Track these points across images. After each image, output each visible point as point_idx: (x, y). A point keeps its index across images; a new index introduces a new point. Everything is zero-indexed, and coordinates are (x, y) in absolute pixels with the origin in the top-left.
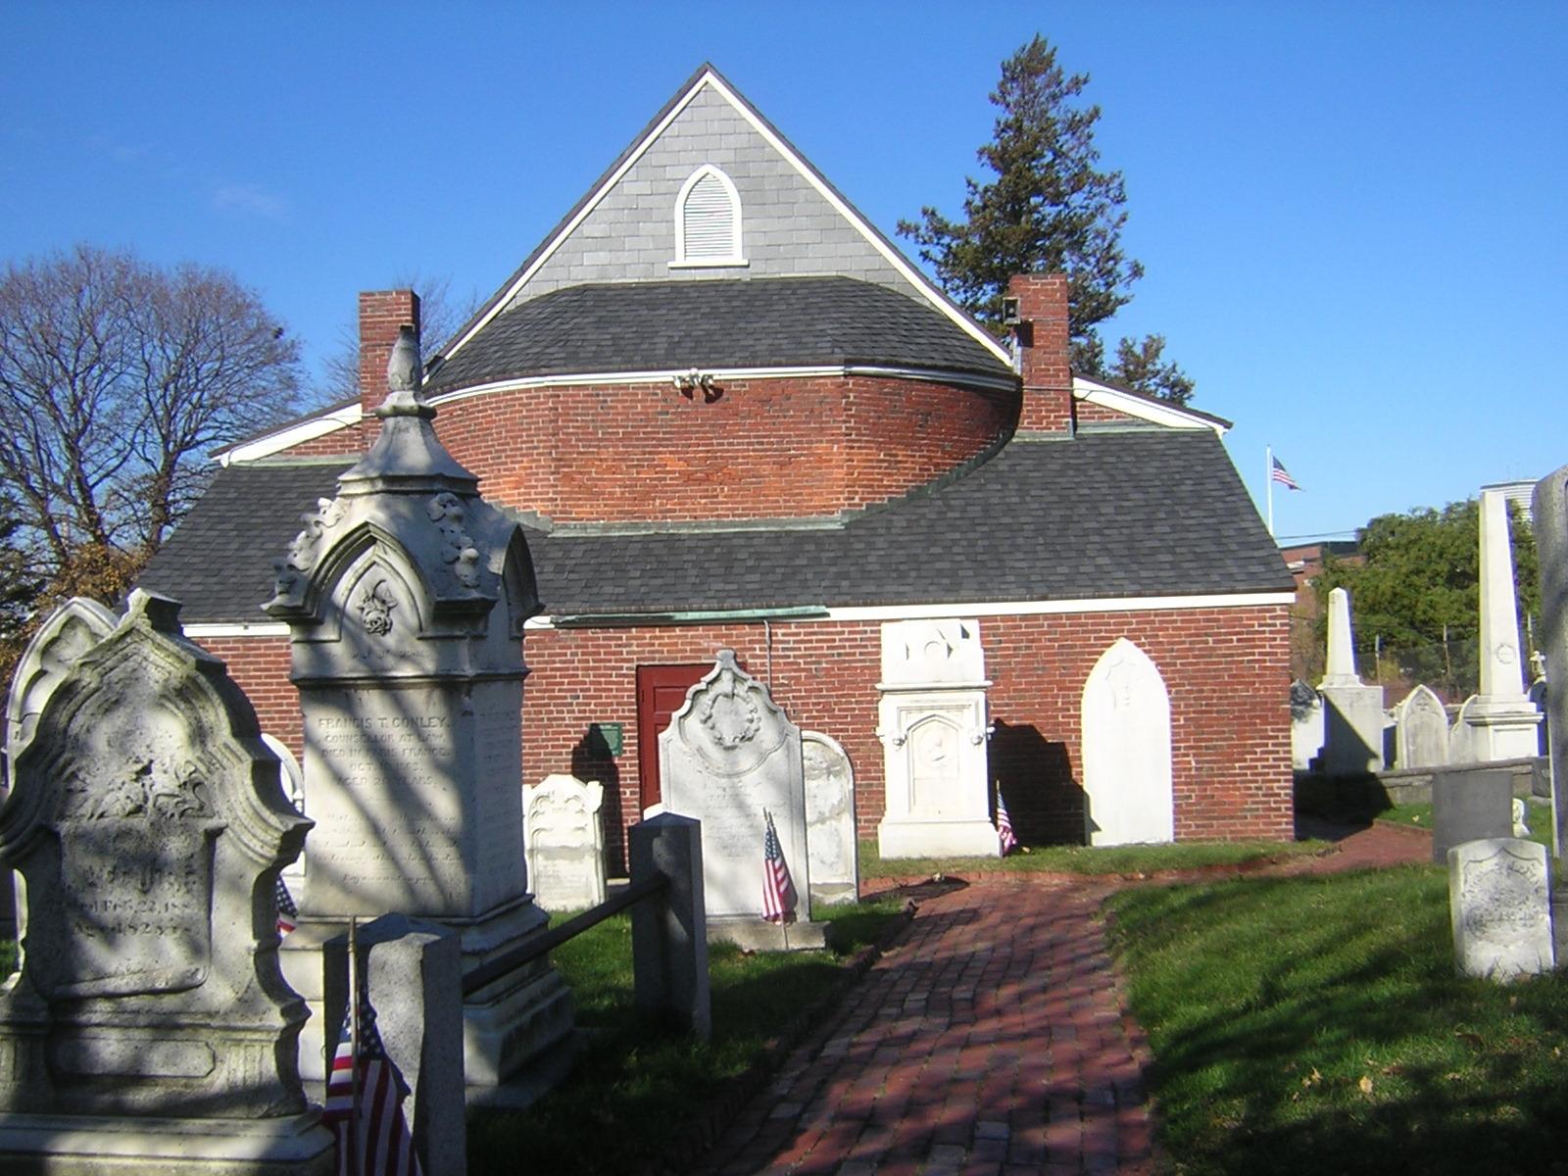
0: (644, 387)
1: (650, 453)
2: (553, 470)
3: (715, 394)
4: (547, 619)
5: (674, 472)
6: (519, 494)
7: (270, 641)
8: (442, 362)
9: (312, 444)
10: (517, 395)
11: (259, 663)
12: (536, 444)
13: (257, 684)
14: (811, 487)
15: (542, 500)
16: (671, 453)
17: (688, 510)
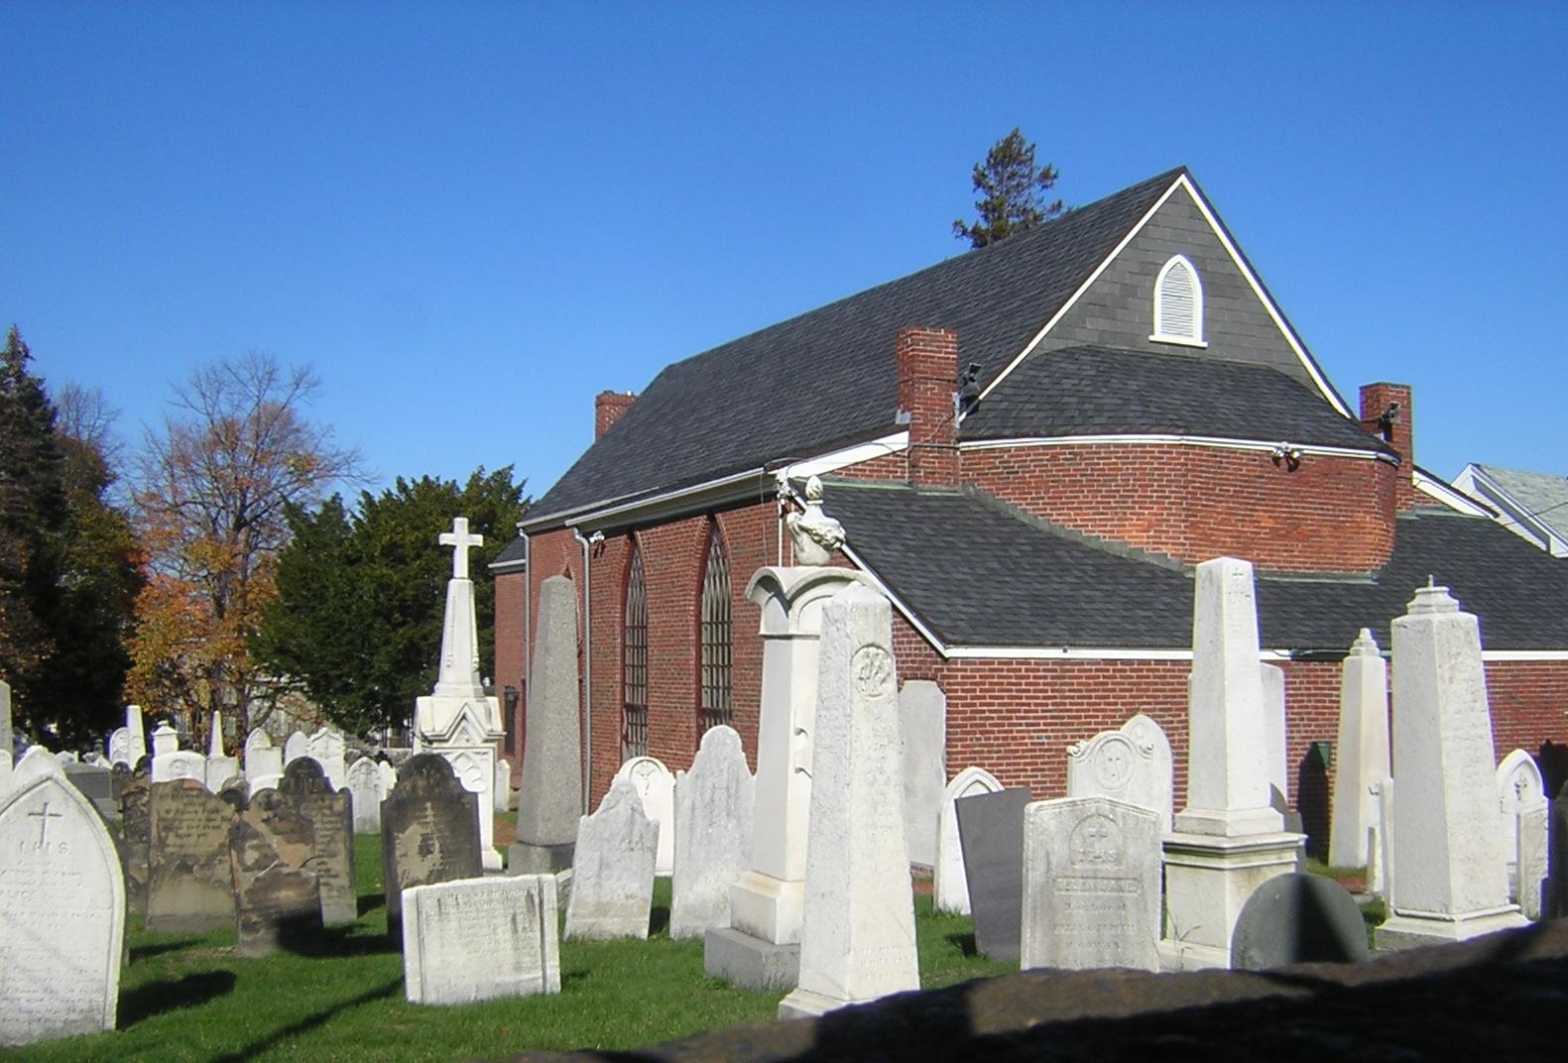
0: (1247, 453)
1: (1251, 510)
2: (1183, 518)
3: (1294, 465)
4: (1286, 652)
5: (1265, 528)
6: (1148, 537)
7: (1082, 664)
8: (976, 402)
9: (860, 467)
10: (1148, 449)
11: (1073, 684)
12: (1167, 494)
13: (1071, 704)
14: (1353, 548)
15: (1173, 544)
16: (1265, 511)
17: (1274, 561)
